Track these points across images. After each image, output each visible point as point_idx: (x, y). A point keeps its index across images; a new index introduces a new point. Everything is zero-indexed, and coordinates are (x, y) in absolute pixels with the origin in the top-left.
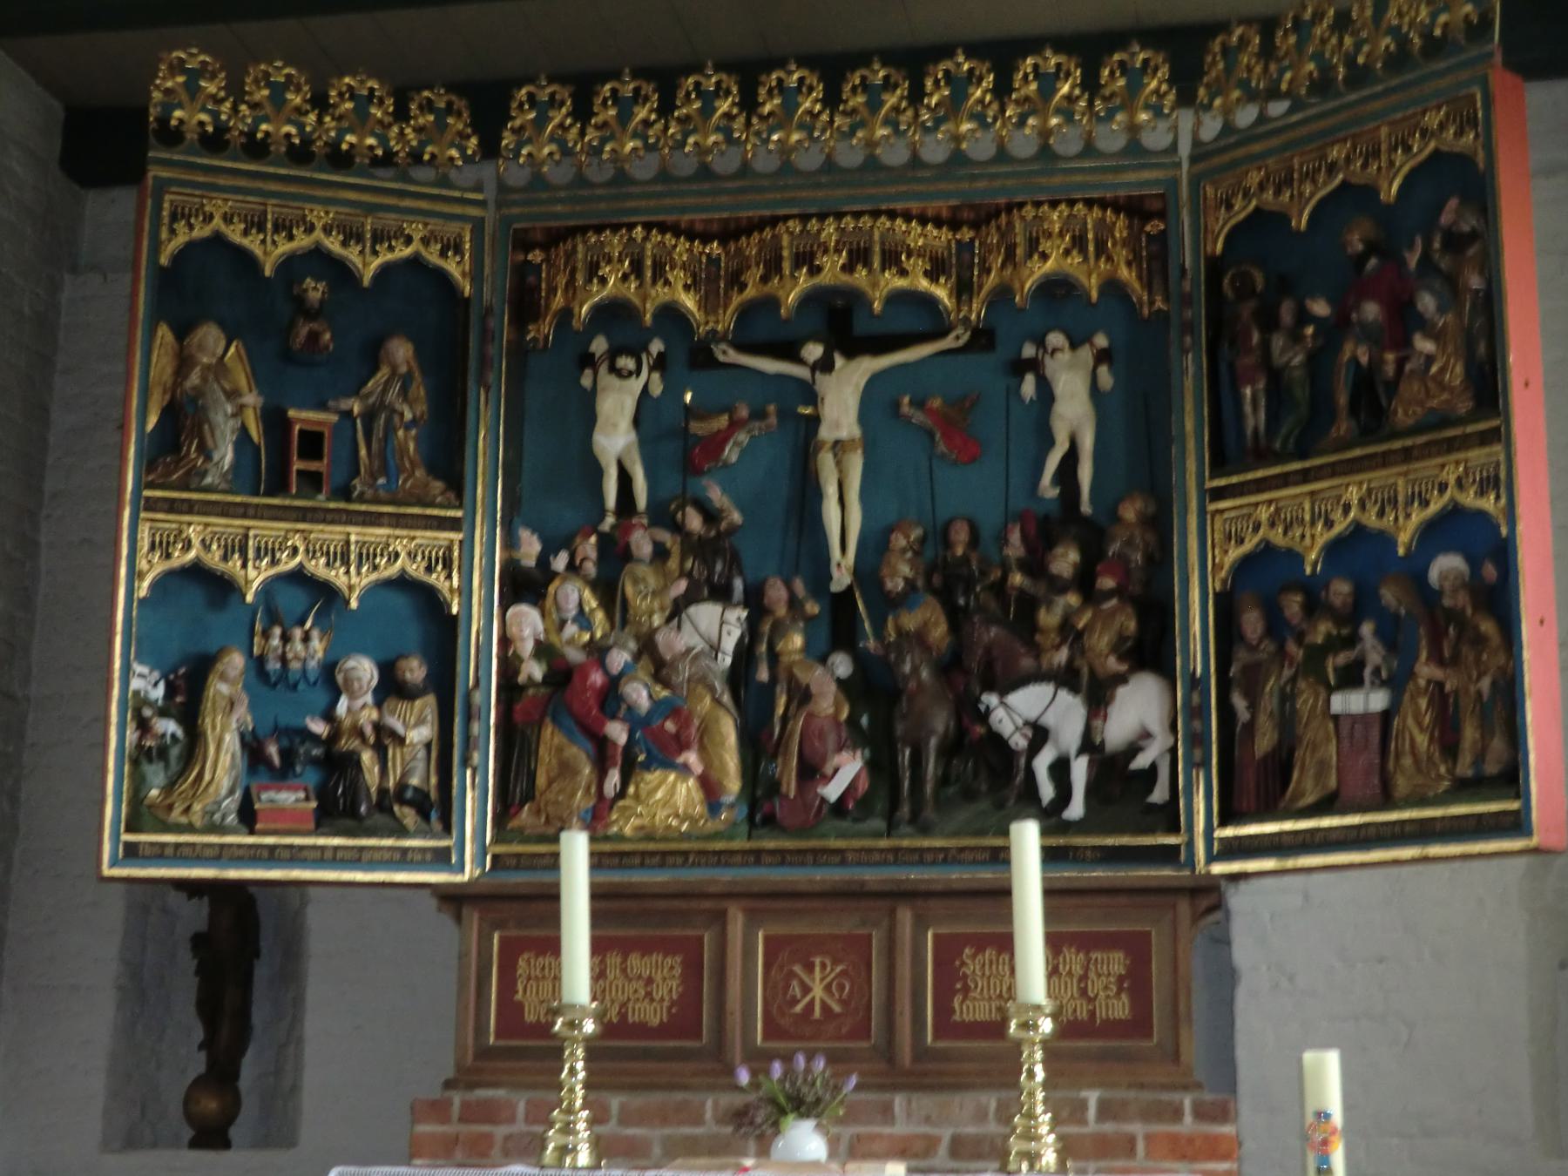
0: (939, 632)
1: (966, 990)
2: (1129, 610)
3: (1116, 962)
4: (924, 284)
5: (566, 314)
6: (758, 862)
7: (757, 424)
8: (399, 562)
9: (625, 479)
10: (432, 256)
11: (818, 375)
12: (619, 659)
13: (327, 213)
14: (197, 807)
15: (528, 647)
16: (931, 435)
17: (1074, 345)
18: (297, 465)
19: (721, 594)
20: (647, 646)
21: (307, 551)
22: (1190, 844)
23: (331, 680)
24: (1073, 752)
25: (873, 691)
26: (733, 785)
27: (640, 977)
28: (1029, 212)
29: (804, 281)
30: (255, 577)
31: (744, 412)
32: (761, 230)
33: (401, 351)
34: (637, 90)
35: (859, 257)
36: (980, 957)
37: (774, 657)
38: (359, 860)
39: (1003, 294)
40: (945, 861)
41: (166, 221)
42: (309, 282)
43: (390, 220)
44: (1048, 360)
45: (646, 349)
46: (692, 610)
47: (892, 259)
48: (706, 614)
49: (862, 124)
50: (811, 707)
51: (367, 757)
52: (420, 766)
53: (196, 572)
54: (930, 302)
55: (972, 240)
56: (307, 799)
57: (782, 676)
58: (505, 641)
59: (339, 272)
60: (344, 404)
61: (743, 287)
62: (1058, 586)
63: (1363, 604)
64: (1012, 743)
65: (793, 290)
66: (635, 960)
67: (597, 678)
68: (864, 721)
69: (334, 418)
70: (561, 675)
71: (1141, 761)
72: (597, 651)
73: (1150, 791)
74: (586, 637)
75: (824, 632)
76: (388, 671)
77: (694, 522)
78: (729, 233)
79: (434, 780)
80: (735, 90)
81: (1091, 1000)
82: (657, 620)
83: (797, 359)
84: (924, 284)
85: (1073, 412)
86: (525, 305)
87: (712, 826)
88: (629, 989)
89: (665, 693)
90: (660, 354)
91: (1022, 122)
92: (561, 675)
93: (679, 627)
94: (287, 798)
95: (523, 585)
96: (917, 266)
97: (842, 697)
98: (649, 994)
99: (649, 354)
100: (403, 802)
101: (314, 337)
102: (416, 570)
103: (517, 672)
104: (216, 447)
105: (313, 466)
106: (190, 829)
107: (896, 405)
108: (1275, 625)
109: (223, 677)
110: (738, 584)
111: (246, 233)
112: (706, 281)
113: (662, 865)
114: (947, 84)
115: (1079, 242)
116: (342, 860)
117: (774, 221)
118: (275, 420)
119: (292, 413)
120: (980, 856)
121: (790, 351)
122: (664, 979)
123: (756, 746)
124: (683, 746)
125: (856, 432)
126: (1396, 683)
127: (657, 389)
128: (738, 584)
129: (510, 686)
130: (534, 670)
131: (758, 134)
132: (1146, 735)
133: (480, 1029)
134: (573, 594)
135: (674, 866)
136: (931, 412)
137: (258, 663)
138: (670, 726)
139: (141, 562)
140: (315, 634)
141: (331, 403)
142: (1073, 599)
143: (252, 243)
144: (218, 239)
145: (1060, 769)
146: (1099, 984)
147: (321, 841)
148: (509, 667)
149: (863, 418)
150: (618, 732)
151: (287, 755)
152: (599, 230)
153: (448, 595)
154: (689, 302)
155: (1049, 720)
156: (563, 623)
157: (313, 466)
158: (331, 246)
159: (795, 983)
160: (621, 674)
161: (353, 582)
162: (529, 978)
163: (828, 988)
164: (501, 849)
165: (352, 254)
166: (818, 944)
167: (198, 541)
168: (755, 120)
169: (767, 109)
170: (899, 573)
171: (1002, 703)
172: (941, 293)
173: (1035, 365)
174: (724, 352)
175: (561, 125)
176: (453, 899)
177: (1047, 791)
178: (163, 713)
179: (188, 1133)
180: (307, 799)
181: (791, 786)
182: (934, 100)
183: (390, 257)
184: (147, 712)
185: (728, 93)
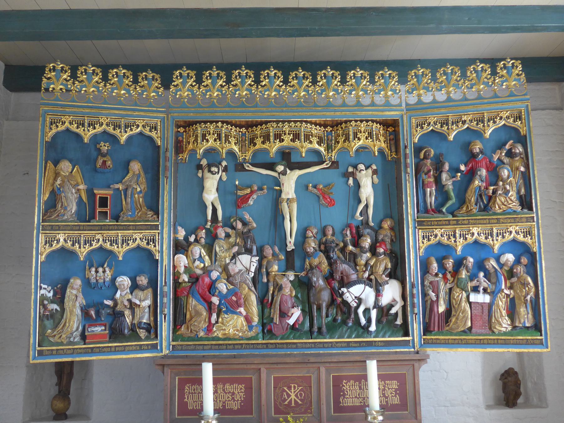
0: (325, 265)
1: (344, 395)
2: (388, 259)
3: (394, 384)
4: (317, 146)
5: (194, 152)
6: (267, 347)
7: (260, 192)
8: (137, 242)
9: (214, 210)
10: (147, 132)
11: (281, 175)
12: (215, 275)
13: (107, 118)
14: (64, 336)
15: (182, 270)
16: (319, 197)
17: (367, 168)
18: (99, 210)
19: (249, 251)
20: (225, 269)
21: (103, 240)
22: (413, 340)
23: (113, 286)
24: (371, 308)
25: (304, 285)
26: (256, 320)
28: (353, 123)
29: (278, 145)
30: (83, 251)
31: (256, 188)
32: (261, 125)
33: (136, 167)
34: (218, 74)
35: (296, 136)
37: (268, 274)
38: (124, 350)
39: (344, 151)
40: (332, 347)
41: (48, 125)
42: (102, 144)
43: (130, 120)
44: (358, 173)
45: (220, 164)
46: (240, 256)
47: (307, 138)
48: (245, 259)
49: (296, 91)
50: (282, 292)
51: (127, 313)
52: (147, 316)
53: (63, 249)
54: (318, 152)
55: (331, 131)
56: (105, 330)
57: (271, 280)
58: (174, 267)
59: (114, 139)
60: (117, 186)
61: (255, 145)
62: (363, 250)
63: (481, 266)
64: (351, 304)
65: (274, 147)
66: (227, 386)
67: (207, 280)
68: (299, 295)
69: (111, 192)
70: (195, 279)
71: (393, 311)
72: (207, 271)
73: (396, 320)
74: (202, 265)
75: (283, 264)
76: (133, 280)
77: (239, 225)
78: (250, 125)
79: (152, 319)
80: (252, 76)
81: (387, 398)
82: (228, 261)
83: (273, 170)
84: (317, 146)
85: (367, 192)
86: (179, 148)
87: (251, 334)
88: (226, 397)
89: (232, 287)
90: (225, 166)
91: (351, 91)
92: (195, 279)
93: (235, 263)
94: (98, 329)
95: (180, 247)
96: (315, 140)
97: (292, 288)
99: (221, 165)
100: (140, 328)
101: (104, 162)
102: (144, 244)
103: (179, 278)
104: (68, 205)
105: (104, 210)
106: (62, 344)
107: (307, 187)
109: (72, 288)
110: (255, 248)
111: (78, 127)
112: (240, 142)
113: (234, 349)
114: (325, 78)
115: (370, 135)
116: (118, 351)
117: (266, 123)
118: (91, 193)
119: (95, 192)
120: (343, 345)
121: (271, 166)
122: (238, 393)
123: (262, 302)
124: (240, 306)
126: (493, 294)
127: (225, 178)
128: (255, 248)
129: (177, 283)
130: (185, 278)
131: (261, 92)
132: (394, 300)
133: (172, 412)
134: (197, 250)
135: (238, 349)
136: (319, 190)
137: (87, 282)
138: (234, 298)
139: (41, 250)
140: (107, 269)
141: (111, 186)
142: (368, 255)
143: (80, 131)
144: (68, 130)
145: (367, 311)
146: (389, 392)
147: (110, 345)
148: (176, 276)
149: (295, 192)
150: (215, 300)
151: (98, 313)
152: (205, 122)
153: (154, 252)
154: (236, 148)
155: (363, 297)
156: (194, 260)
157: (104, 210)
158: (109, 130)
160: (216, 280)
161: (120, 251)
162: (189, 393)
163: (296, 396)
164: (174, 343)
165: (117, 132)
166: (293, 380)
167: (61, 239)
168: (260, 87)
169: (263, 83)
170: (312, 245)
171: (348, 291)
172: (322, 149)
173: (353, 174)
174: (248, 167)
175: (191, 85)
176: (162, 365)
177: (363, 321)
178: (52, 302)
179: (52, 414)
180: (105, 330)
181: (277, 319)
182: (321, 83)
183: (131, 133)
184: (46, 302)
185: (250, 77)
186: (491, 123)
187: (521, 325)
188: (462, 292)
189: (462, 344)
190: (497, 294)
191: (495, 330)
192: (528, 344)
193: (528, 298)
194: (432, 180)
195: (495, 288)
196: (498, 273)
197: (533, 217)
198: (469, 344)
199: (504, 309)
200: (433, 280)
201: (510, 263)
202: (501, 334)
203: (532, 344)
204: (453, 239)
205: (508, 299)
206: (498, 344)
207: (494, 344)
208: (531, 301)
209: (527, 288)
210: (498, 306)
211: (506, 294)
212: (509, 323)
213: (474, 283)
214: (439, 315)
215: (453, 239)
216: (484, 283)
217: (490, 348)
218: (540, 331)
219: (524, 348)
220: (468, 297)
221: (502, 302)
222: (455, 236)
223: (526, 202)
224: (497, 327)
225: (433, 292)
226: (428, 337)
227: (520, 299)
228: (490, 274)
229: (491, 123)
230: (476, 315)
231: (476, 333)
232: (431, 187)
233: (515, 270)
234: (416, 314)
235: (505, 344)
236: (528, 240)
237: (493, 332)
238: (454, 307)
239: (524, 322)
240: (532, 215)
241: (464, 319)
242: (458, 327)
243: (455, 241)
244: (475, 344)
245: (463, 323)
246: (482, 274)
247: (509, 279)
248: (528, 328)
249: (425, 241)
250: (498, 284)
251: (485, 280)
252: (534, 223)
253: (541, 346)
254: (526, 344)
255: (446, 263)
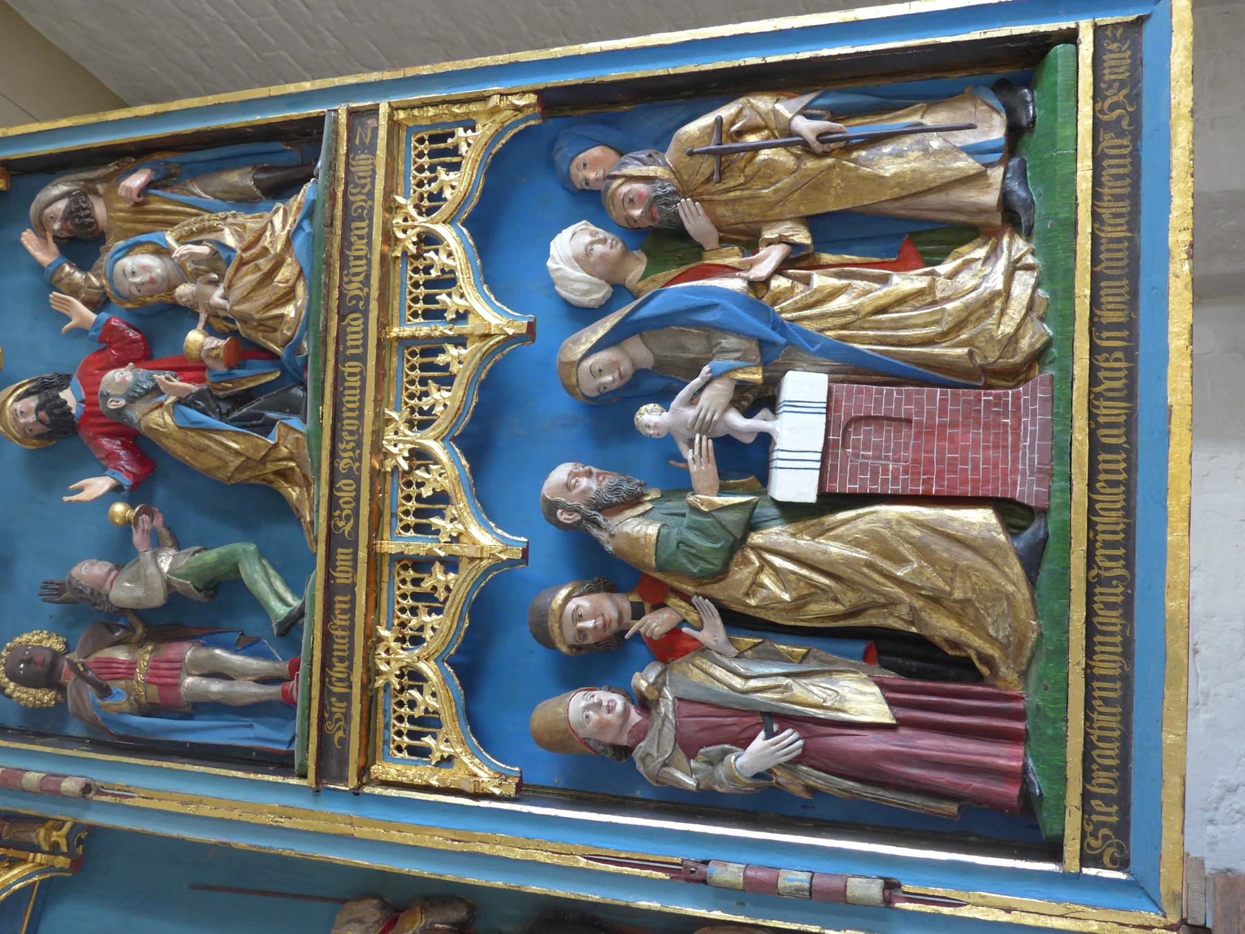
126: (778, 350)
186: (450, 301)
187: (997, 174)
188: (757, 549)
189: (1129, 583)
190: (778, 325)
191: (1024, 344)
192: (1136, 119)
193: (804, 126)
194: (145, 657)
195: (738, 333)
196: (645, 312)
197: (352, 113)
198: (1130, 531)
199: (884, 280)
200: (669, 731)
201: (607, 246)
202: (1054, 302)
203: (1135, 98)
204: (439, 575)
205: (827, 258)
206: (1130, 326)
207: (1131, 354)
208: (836, 114)
209: (752, 139)
210: (852, 318)
211: (779, 271)
212: (981, 253)
213: (699, 462)
214: (902, 723)
215: (439, 575)
216: (688, 414)
217: (1162, 378)
218: (1039, 46)
219: (1166, 143)
220: (792, 512)
221: (834, 294)
222: (422, 564)
223: (282, 155)
224: (1007, 328)
225: (745, 744)
226: (1073, 824)
227: (817, 184)
228: (661, 367)
229: (450, 301)
230: (913, 469)
231: (1046, 474)
232: (178, 667)
233: (637, 212)
234: (891, 886)
235: (1133, 274)
236: (471, 144)
237: (1039, 357)
238: (854, 613)
239: (973, 151)
240: (343, 119)
241: (938, 545)
242: (1000, 595)
243: (451, 564)
244: (1129, 488)
245: (967, 558)
246: (650, 416)
247: (698, 250)
248: (1016, 132)
249: (439, 747)
250: (708, 317)
251: (684, 393)
252: (384, 109)
253: (1148, 28)
254: (1136, 135)
255: (570, 634)
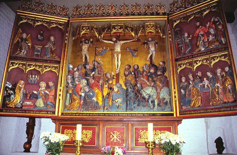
27: (85, 134)
36: (143, 131)
68: (38, 79)
98: (86, 137)
99: (90, 41)
108: (188, 80)
125: (120, 51)
149: (121, 50)
159: (111, 135)
166: (115, 129)
